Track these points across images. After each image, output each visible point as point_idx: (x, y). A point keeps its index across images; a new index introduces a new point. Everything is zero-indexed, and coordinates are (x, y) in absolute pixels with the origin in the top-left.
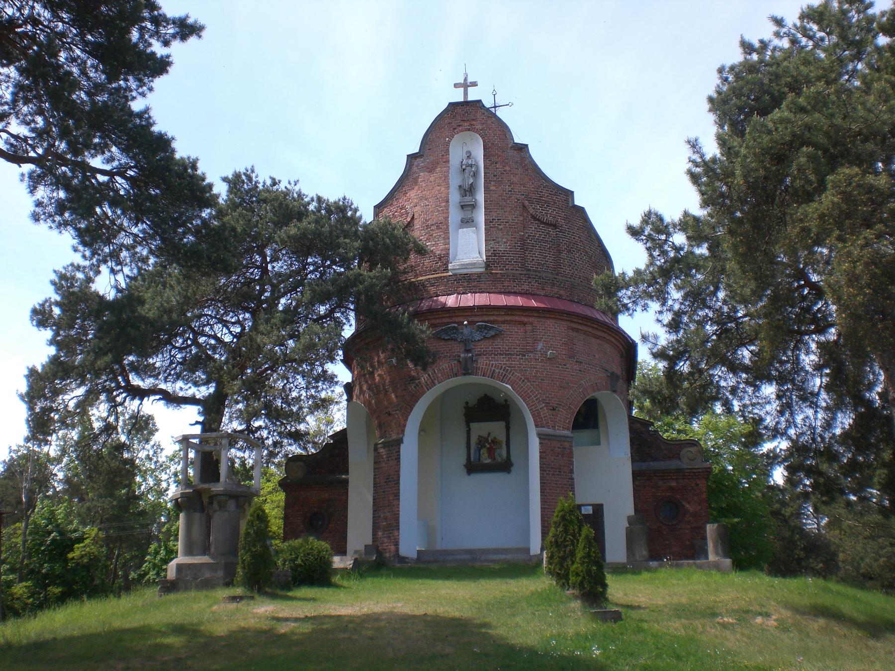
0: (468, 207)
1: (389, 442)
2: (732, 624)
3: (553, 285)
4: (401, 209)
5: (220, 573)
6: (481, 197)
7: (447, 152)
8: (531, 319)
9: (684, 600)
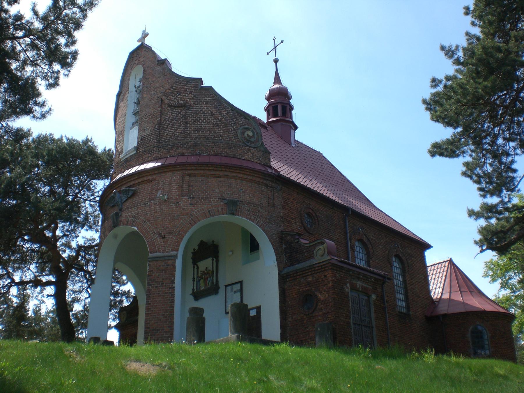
8: (154, 176)
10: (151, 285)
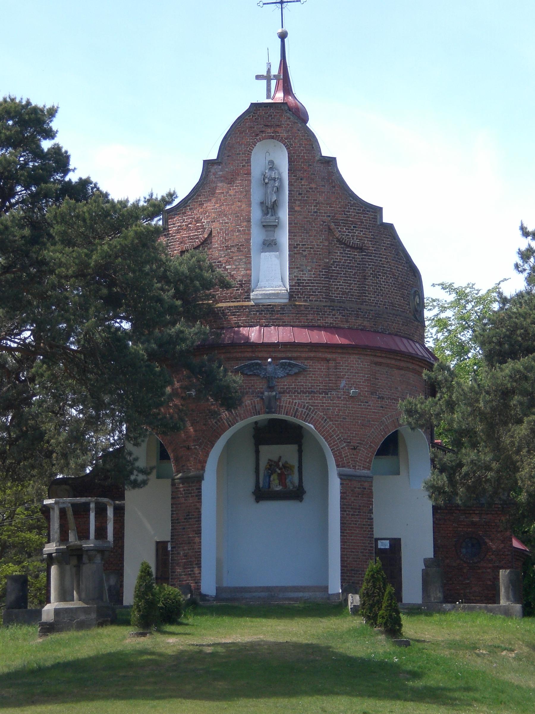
0: (270, 227)
1: (188, 478)
2: (484, 655)
3: (357, 316)
4: (197, 221)
5: (93, 616)
6: (284, 215)
7: (249, 161)
8: (334, 356)
9: (458, 638)
10: (345, 511)
